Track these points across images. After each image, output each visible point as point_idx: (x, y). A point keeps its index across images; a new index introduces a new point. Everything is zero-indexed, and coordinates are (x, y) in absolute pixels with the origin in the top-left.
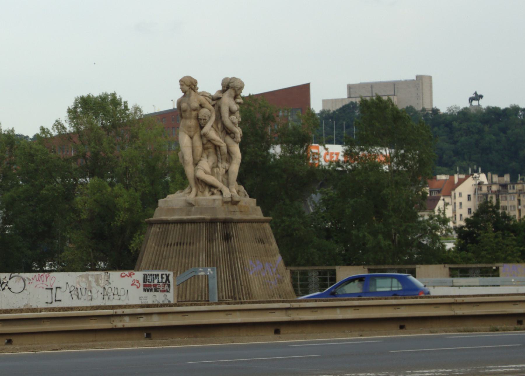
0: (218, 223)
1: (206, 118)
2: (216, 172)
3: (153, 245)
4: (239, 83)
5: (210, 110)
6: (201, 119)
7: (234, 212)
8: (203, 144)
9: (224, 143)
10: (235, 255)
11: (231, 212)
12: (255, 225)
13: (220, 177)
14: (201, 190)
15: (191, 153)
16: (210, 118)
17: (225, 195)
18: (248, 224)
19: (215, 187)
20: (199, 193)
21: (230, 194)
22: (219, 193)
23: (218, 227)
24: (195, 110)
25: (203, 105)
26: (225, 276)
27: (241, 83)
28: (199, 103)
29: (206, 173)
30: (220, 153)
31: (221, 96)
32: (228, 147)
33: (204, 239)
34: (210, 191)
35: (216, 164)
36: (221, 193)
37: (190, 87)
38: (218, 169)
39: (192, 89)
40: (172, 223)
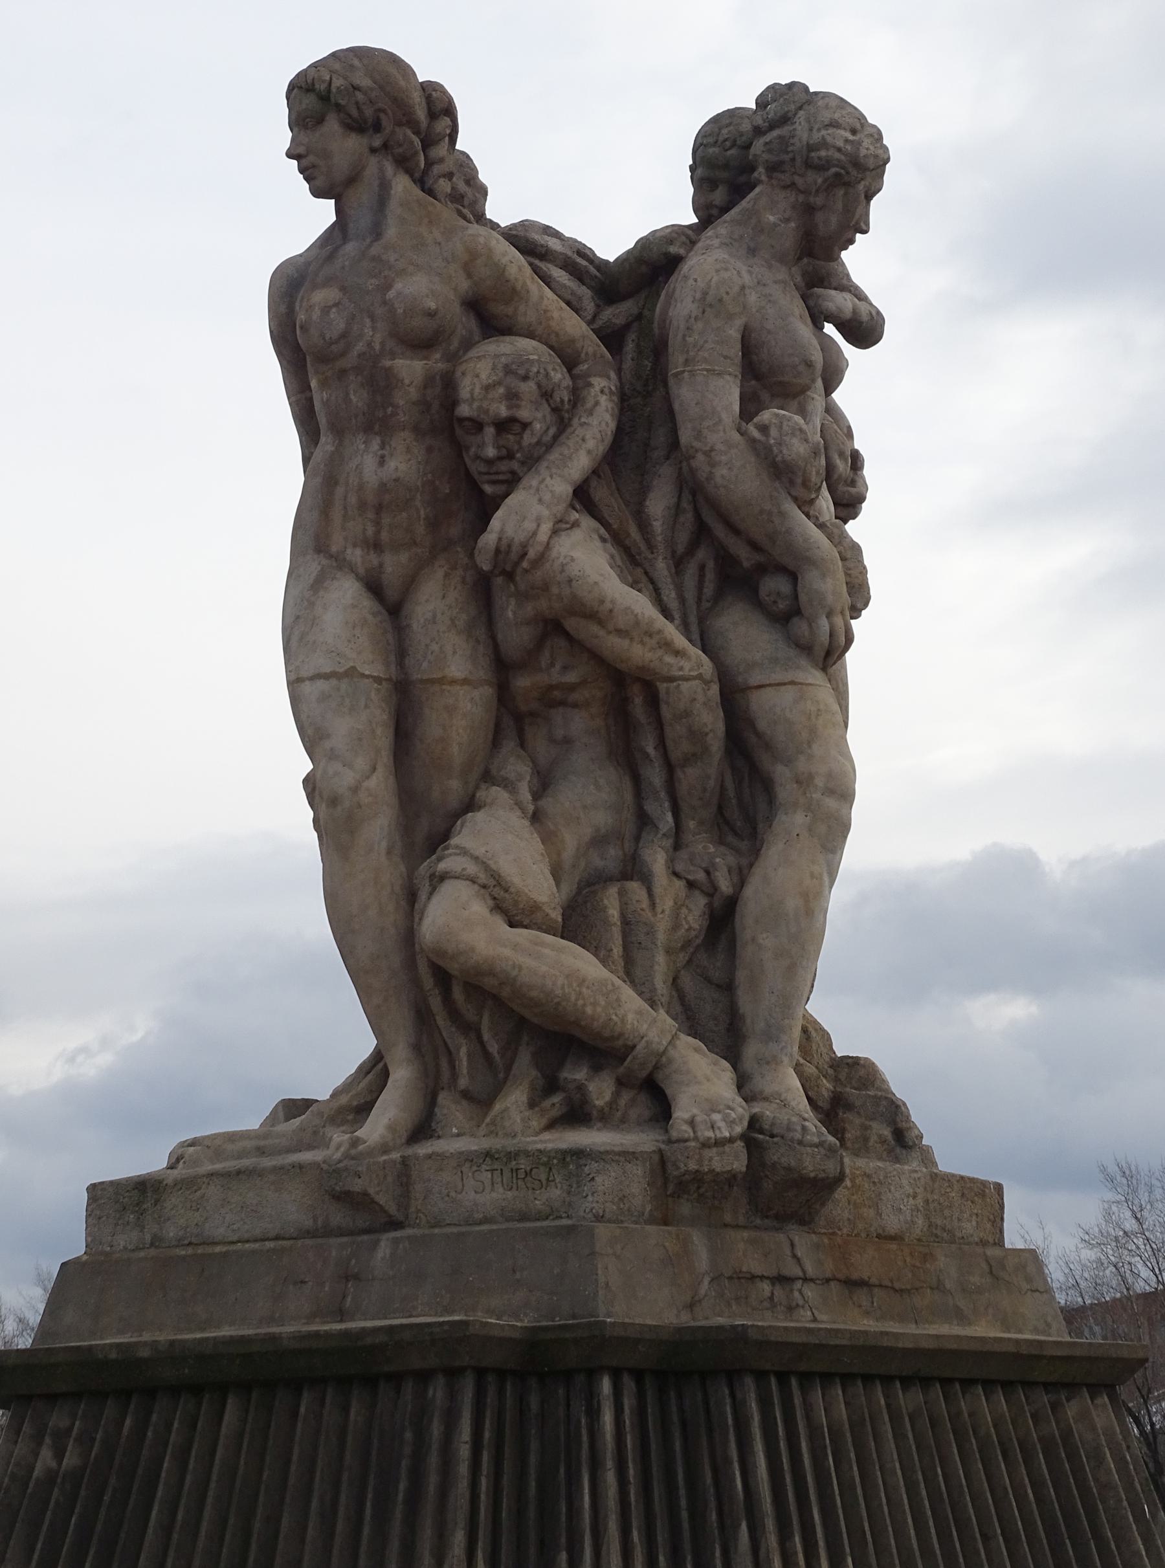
1: (524, 414)
2: (614, 913)
5: (570, 362)
6: (477, 426)
9: (695, 652)
13: (661, 967)
15: (384, 739)
16: (563, 420)
17: (692, 1123)
18: (909, 1400)
20: (451, 1109)
21: (741, 1110)
22: (642, 1107)
23: (608, 1418)
24: (422, 344)
27: (854, 132)
31: (733, 332)
34: (551, 1085)
37: (377, 142)
38: (635, 888)
39: (404, 163)
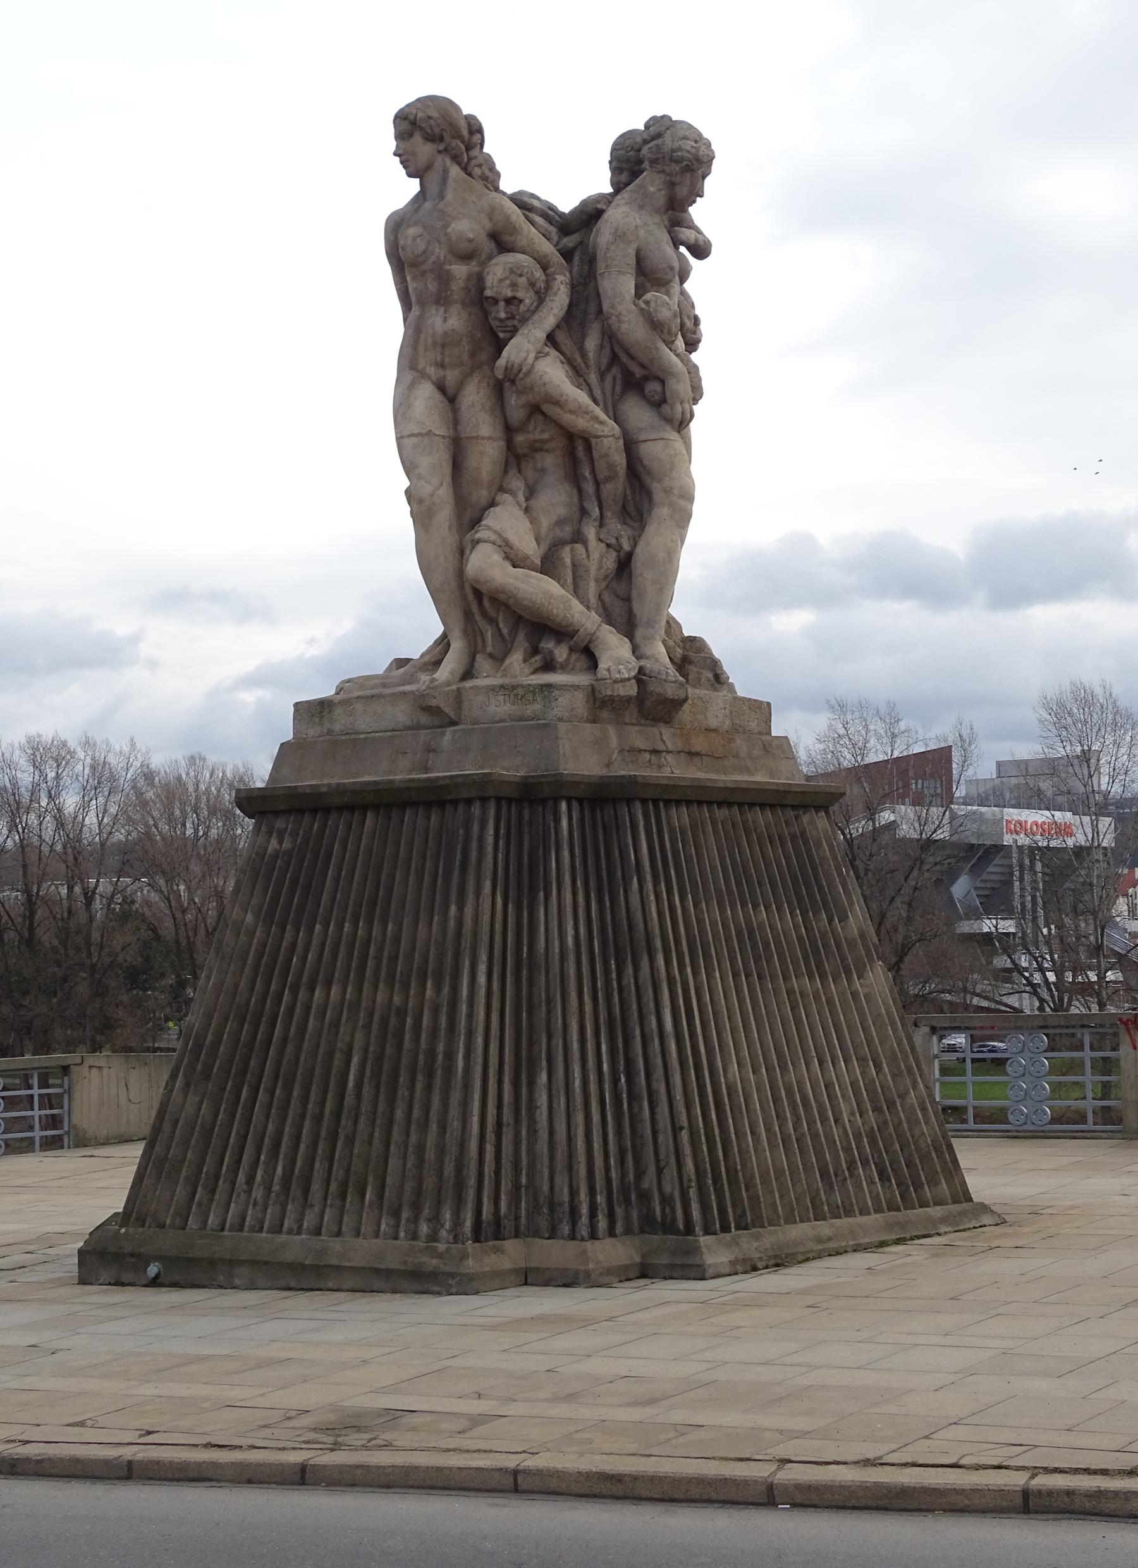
0: (564, 806)
3: (249, 918)
4: (685, 138)
6: (496, 301)
7: (655, 752)
8: (509, 431)
9: (611, 422)
10: (645, 962)
11: (640, 751)
12: (761, 818)
13: (592, 589)
14: (489, 649)
16: (541, 297)
19: (562, 633)
21: (634, 664)
23: (564, 823)
24: (466, 257)
25: (507, 238)
26: (592, 1077)
27: (696, 142)
28: (488, 225)
29: (517, 562)
30: (593, 471)
32: (630, 446)
33: (487, 885)
35: (568, 529)
36: (589, 656)
38: (579, 547)
39: (456, 159)
40: (340, 809)
